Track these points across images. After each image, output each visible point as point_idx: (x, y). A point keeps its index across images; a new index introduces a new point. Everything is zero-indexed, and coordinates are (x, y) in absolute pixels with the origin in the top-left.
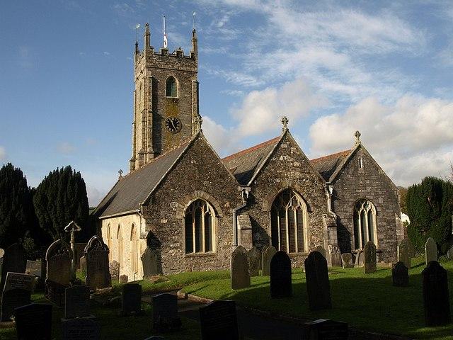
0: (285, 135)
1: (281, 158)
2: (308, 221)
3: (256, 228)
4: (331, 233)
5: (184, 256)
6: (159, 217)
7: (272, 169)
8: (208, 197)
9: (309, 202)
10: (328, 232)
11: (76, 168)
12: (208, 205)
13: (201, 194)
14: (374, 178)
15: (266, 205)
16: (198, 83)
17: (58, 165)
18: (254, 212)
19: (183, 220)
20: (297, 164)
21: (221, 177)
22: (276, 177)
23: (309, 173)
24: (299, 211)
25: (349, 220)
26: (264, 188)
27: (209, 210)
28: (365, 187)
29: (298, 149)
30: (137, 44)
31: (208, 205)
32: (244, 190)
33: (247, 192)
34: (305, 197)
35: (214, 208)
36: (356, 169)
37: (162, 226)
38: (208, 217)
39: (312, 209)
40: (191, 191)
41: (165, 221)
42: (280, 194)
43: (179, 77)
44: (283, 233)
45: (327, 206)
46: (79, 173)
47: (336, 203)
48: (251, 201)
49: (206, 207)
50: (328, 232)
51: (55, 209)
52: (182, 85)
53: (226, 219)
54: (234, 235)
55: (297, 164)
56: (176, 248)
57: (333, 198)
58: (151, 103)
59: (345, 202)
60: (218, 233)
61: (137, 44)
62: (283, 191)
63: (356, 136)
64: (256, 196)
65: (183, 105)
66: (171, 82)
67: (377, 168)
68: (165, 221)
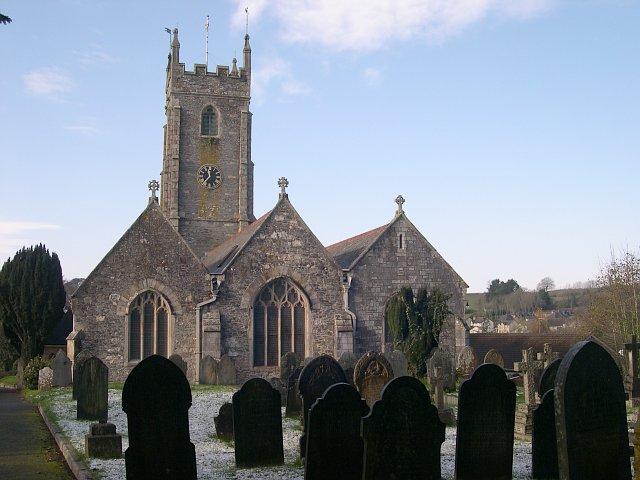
0: (281, 203)
1: (274, 235)
2: (312, 323)
3: (225, 330)
4: (344, 341)
5: (125, 364)
6: (94, 313)
7: (259, 251)
8: (161, 288)
9: (314, 296)
10: (339, 339)
11: (51, 250)
12: (162, 299)
13: (153, 283)
14: (422, 263)
15: (246, 301)
16: (249, 115)
17: (30, 243)
18: (229, 310)
19: (127, 317)
20: (298, 243)
21: (182, 261)
22: (264, 261)
23: (316, 256)
24: (299, 310)
25: (378, 323)
26: (244, 275)
27: (301, 299)
28: (407, 276)
29: (301, 222)
30: (247, 38)
31: (162, 299)
32: (215, 279)
33: (219, 283)
34: (308, 289)
35: (169, 303)
36: (393, 250)
37: (97, 324)
38: (162, 314)
39: (318, 306)
40: (138, 280)
41: (101, 319)
42: (270, 284)
43: (221, 106)
44: (272, 338)
45: (342, 302)
46: (55, 256)
47: (358, 299)
48: (224, 295)
49: (159, 300)
50: (339, 339)
51: (19, 299)
52: (226, 119)
53: (187, 318)
54: (197, 339)
55: (298, 243)
56: (116, 354)
57: (352, 292)
58: (177, 146)
59: (372, 298)
60: (176, 336)
61: (247, 38)
62: (275, 281)
63: (397, 201)
64: (234, 286)
65: (227, 148)
66: (209, 114)
67: (429, 249)
68: (101, 319)
